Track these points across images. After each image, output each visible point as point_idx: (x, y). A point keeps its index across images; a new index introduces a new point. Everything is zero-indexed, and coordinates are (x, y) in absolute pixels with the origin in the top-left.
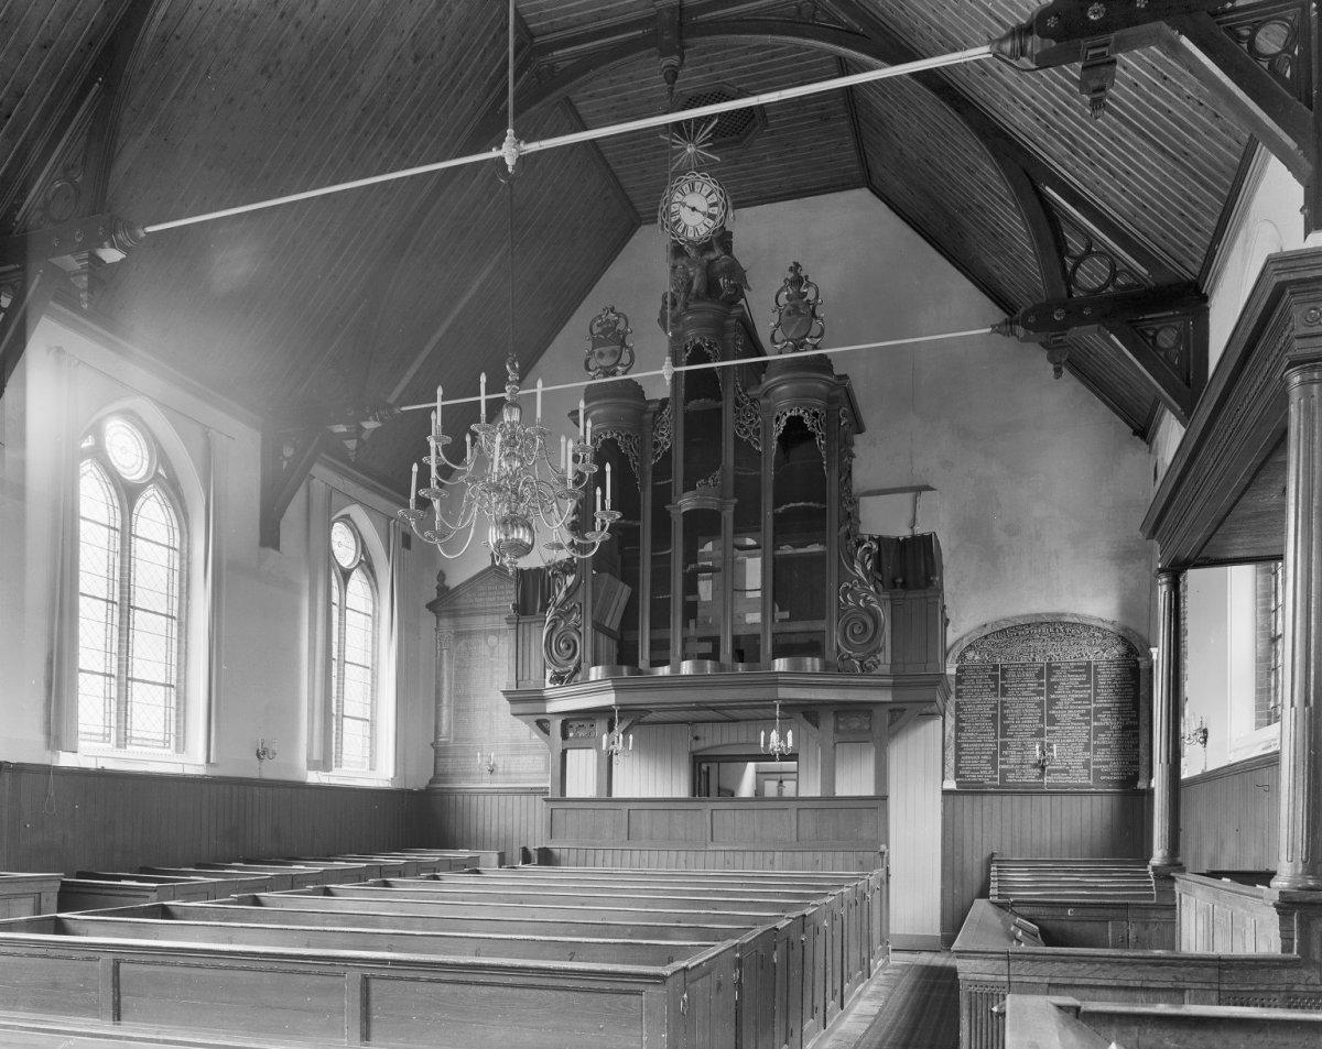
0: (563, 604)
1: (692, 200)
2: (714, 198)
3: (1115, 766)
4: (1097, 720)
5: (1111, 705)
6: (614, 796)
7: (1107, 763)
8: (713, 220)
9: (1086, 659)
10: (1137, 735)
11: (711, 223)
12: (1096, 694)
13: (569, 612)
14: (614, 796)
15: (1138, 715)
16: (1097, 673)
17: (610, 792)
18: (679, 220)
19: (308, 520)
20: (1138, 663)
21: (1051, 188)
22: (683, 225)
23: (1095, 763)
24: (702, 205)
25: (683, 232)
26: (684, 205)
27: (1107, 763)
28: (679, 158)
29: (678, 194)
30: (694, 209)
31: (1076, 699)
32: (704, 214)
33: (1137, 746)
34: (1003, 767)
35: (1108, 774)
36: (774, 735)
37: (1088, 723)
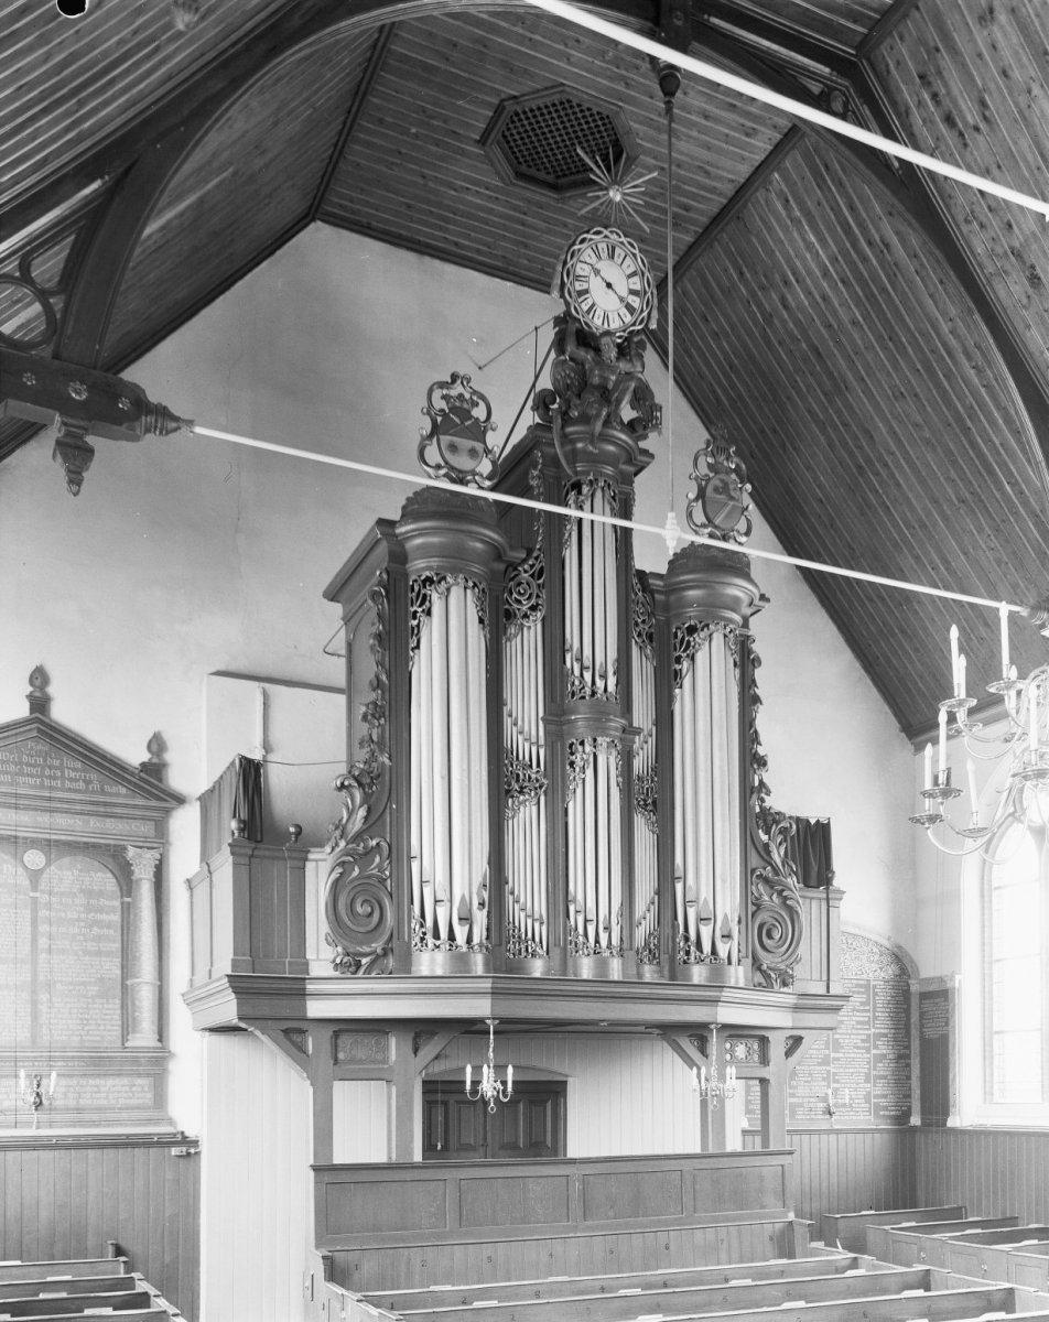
0: (358, 837)
1: (610, 271)
2: (636, 284)
3: (891, 1098)
4: (876, 1047)
5: (886, 1031)
6: (832, 992)
7: (885, 1096)
8: (632, 315)
9: (865, 976)
10: (908, 1065)
11: (628, 319)
12: (875, 1018)
13: (369, 852)
14: (832, 992)
15: (909, 1042)
16: (876, 994)
17: (828, 992)
18: (593, 305)
19: (468, 719)
20: (908, 985)
21: (717, 17)
22: (590, 302)
23: (876, 1097)
24: (622, 287)
25: (588, 312)
26: (597, 272)
27: (885, 1096)
28: (598, 197)
29: (589, 251)
30: (609, 285)
31: (858, 1023)
32: (622, 299)
33: (909, 1078)
34: (793, 1100)
35: (886, 1108)
36: (487, 1073)
37: (868, 1050)
